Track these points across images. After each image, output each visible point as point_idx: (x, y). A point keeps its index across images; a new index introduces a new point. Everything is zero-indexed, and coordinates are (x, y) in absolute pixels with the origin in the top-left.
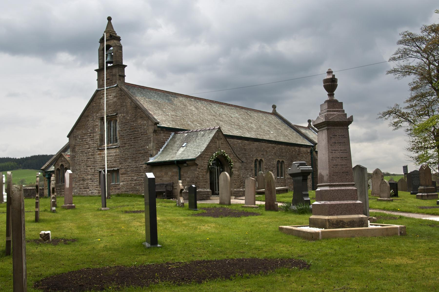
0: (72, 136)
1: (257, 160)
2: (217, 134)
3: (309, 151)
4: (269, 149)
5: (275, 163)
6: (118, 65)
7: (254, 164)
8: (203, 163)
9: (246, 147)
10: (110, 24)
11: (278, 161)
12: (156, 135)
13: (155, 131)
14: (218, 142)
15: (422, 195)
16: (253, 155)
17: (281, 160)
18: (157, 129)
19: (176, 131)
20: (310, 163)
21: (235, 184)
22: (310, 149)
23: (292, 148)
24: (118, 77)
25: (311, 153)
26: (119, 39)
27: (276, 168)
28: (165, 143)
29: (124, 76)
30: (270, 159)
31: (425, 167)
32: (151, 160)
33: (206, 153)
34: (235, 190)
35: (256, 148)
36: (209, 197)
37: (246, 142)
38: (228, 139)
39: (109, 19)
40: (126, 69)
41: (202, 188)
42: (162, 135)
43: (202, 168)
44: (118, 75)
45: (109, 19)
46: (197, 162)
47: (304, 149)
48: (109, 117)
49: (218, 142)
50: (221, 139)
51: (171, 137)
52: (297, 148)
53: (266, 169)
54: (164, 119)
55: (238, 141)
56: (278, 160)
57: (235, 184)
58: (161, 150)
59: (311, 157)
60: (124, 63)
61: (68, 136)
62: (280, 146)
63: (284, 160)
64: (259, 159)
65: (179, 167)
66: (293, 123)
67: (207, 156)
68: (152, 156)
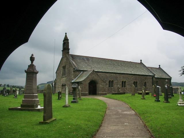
10: (66, 36)
25: (152, 78)
26: (68, 40)
39: (66, 33)
45: (66, 33)
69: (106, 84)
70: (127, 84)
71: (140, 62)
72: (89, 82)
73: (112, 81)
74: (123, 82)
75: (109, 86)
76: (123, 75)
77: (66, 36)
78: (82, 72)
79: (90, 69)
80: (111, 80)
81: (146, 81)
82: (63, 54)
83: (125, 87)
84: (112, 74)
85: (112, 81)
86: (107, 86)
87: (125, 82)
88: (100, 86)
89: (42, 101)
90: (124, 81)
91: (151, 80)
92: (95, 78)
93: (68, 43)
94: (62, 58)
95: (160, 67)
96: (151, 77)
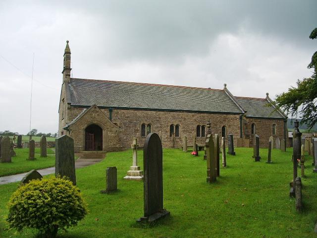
5: (195, 127)
10: (68, 47)
25: (241, 118)
39: (68, 42)
45: (68, 42)
69: (137, 131)
70: (180, 129)
71: (265, 97)
74: (172, 126)
75: (198, 135)
76: (172, 113)
77: (68, 47)
78: (85, 109)
81: (225, 124)
84: (149, 112)
85: (149, 125)
87: (177, 127)
88: (108, 135)
89: (289, 174)
90: (175, 124)
91: (238, 123)
92: (100, 118)
95: (268, 97)
96: (238, 116)
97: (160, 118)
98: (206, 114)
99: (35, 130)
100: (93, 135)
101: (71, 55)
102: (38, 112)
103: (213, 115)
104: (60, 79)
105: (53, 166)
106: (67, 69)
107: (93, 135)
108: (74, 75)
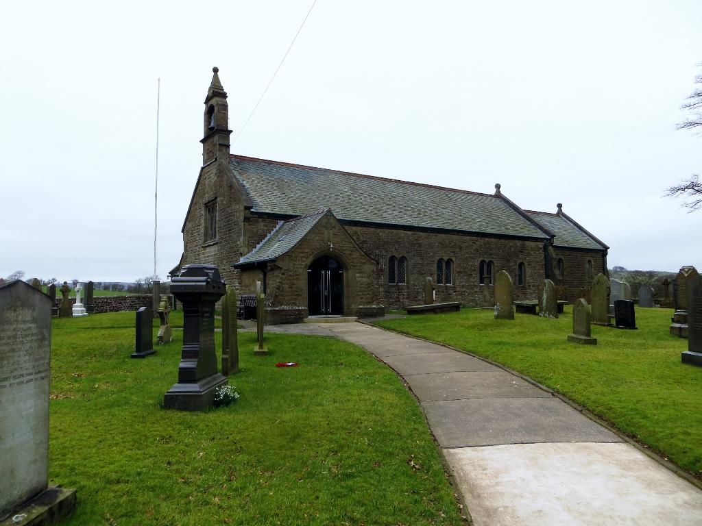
0: (185, 231)
1: (440, 261)
2: (325, 221)
3: (541, 246)
4: (466, 244)
5: (477, 263)
6: (221, 130)
7: (435, 266)
8: (291, 265)
9: (420, 242)
10: (216, 80)
11: (482, 262)
12: (250, 225)
13: (246, 219)
14: (326, 232)
15: (680, 328)
16: (434, 253)
17: (487, 260)
18: (249, 215)
19: (286, 218)
20: (544, 263)
21: (362, 298)
22: (543, 244)
23: (511, 243)
24: (218, 146)
25: (545, 248)
26: (224, 96)
27: (478, 271)
28: (266, 236)
29: (228, 146)
30: (467, 258)
31: (687, 272)
32: (242, 260)
33: (299, 250)
34: (361, 307)
35: (441, 243)
36: (302, 318)
37: (421, 233)
38: (346, 227)
39: (216, 70)
40: (231, 136)
41: (287, 305)
42: (261, 225)
43: (290, 273)
44: (218, 143)
45: (216, 70)
46: (279, 264)
47: (533, 244)
48: (329, 214)
49: (326, 232)
50: (334, 227)
51: (278, 227)
52: (518, 243)
53: (459, 272)
54: (266, 202)
55: (406, 232)
56: (482, 259)
57: (362, 298)
58: (258, 246)
59: (545, 255)
60: (230, 129)
61: (183, 231)
62: (487, 239)
63: (493, 260)
64: (446, 258)
65: (262, 270)
66: (524, 206)
67: (302, 255)
68: (241, 255)
70: (454, 267)
72: (309, 261)
73: (402, 259)
75: (392, 279)
77: (216, 80)
79: (312, 209)
80: (398, 256)
82: (209, 155)
83: (401, 280)
85: (402, 259)
86: (383, 279)
87: (449, 262)
88: (358, 277)
91: (541, 257)
93: (225, 107)
94: (203, 168)
96: (541, 245)
97: (420, 245)
98: (493, 240)
99: (19, 273)
100: (686, 275)
101: (228, 100)
102: (137, 233)
103: (503, 241)
104: (192, 159)
105: (180, 327)
106: (216, 130)
107: (686, 275)
108: (239, 146)
